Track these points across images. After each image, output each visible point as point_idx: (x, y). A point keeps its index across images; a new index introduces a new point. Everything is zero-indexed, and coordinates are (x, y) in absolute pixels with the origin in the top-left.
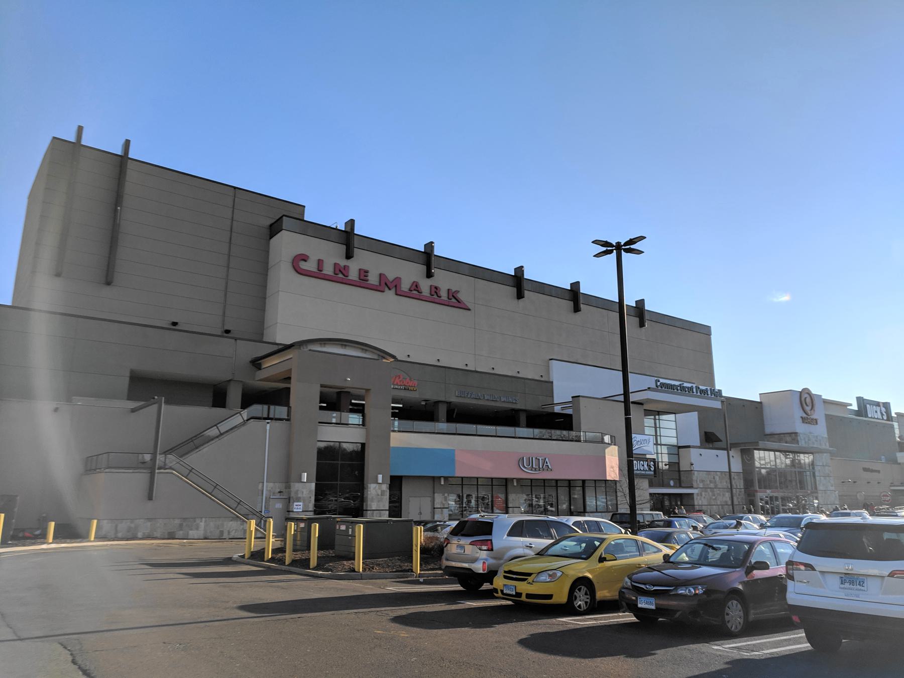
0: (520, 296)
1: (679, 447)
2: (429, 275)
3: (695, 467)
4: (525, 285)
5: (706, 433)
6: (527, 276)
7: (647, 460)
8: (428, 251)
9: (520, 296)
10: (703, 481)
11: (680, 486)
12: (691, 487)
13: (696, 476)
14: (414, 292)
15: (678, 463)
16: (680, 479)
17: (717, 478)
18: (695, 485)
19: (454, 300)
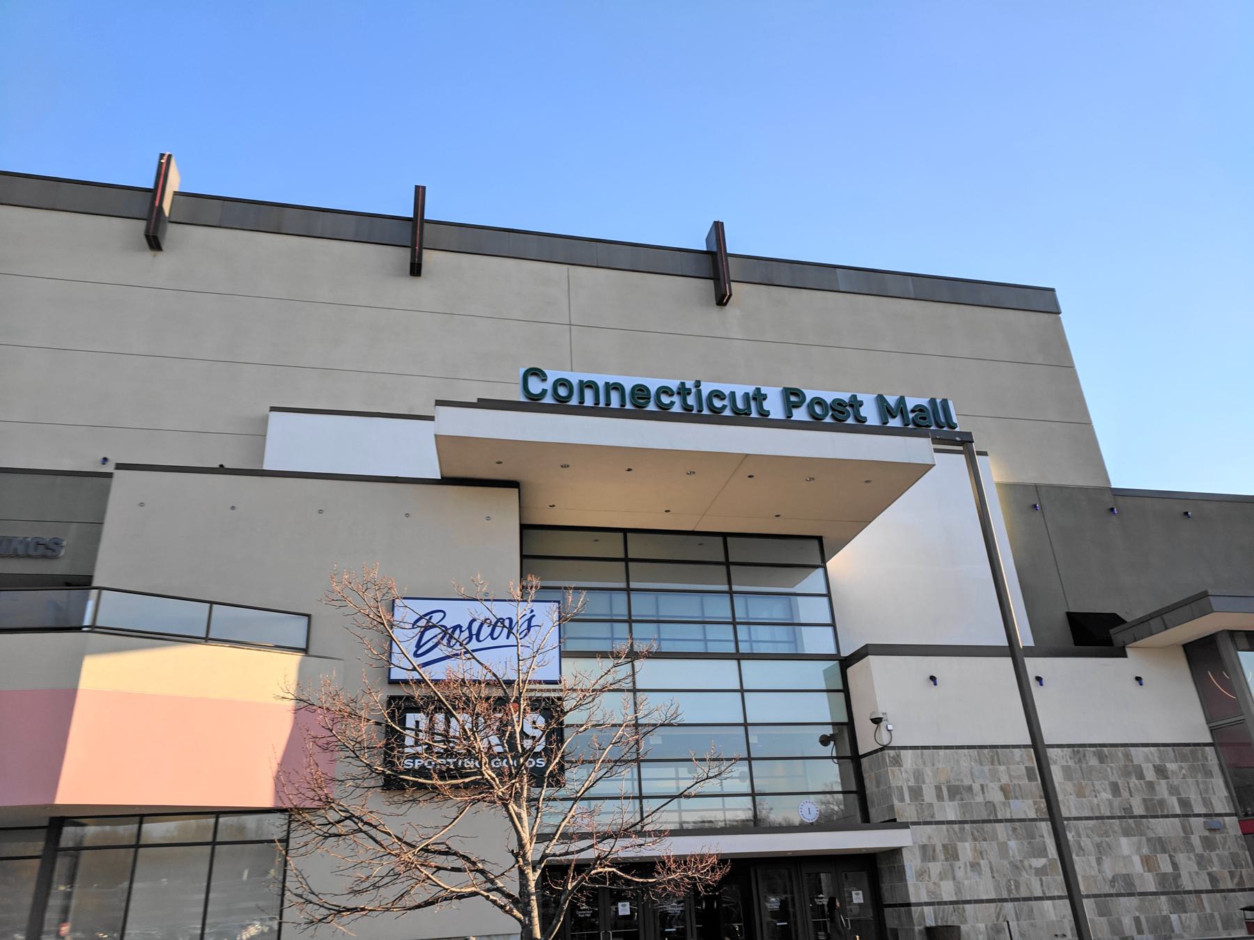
1: (845, 663)
4: (734, 268)
6: (734, 245)
13: (900, 777)
18: (906, 810)
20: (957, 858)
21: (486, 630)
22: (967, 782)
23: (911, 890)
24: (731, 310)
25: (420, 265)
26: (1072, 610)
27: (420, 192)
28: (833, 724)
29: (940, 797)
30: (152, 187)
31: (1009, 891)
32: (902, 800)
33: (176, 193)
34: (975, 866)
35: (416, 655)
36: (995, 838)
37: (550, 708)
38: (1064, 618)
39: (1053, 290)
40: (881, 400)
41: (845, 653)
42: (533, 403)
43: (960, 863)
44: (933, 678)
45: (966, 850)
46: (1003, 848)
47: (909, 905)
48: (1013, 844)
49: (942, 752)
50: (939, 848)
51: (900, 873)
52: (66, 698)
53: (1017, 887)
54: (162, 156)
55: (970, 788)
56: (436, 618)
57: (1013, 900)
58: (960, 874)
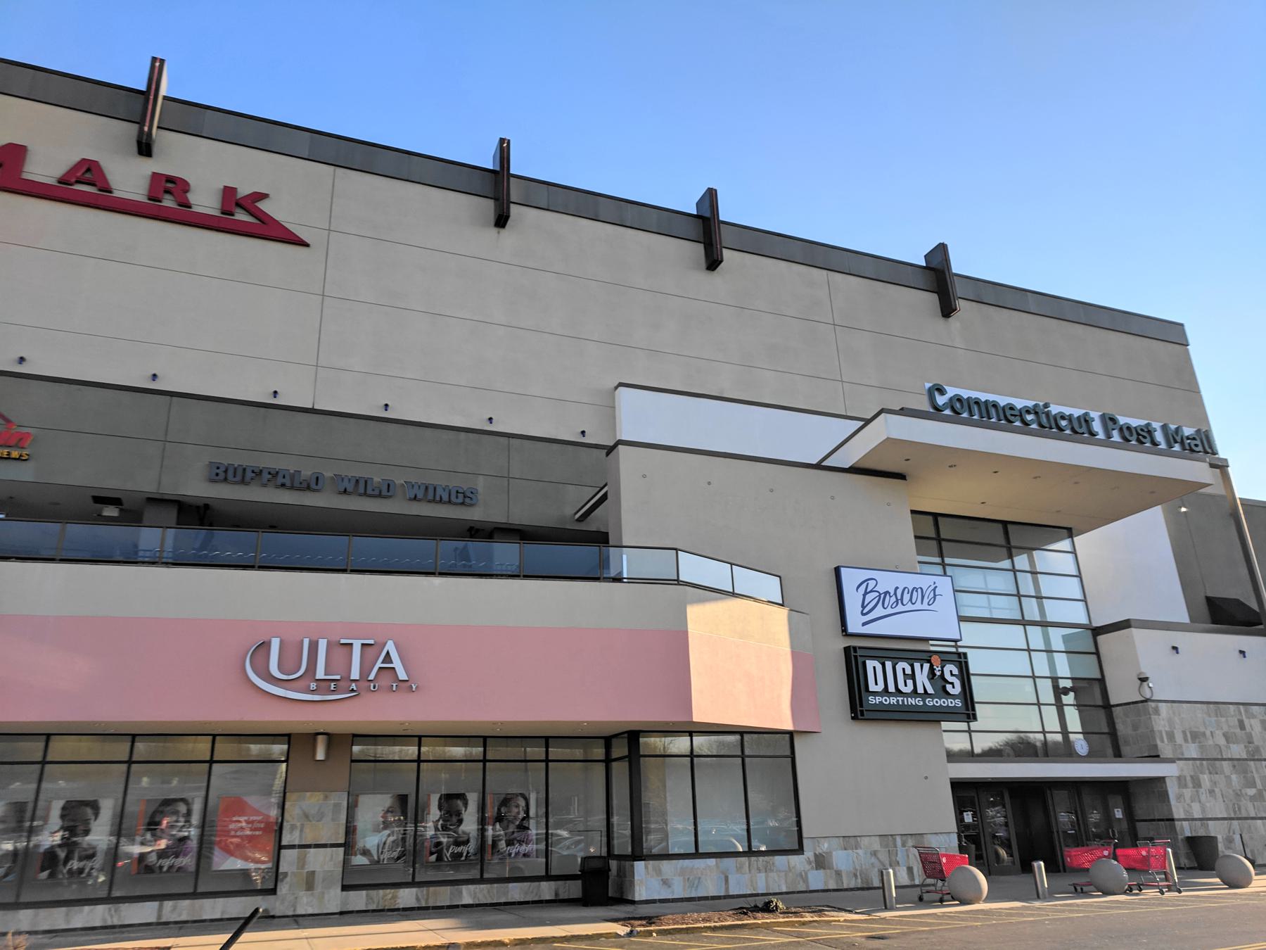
0: (947, 310)
1: (1097, 632)
2: (145, 148)
3: (1160, 689)
4: (726, 236)
5: (1209, 600)
6: (726, 213)
7: (926, 657)
8: (707, 214)
9: (947, 310)
10: (1196, 736)
11: (1118, 755)
12: (1155, 757)
13: (1161, 721)
14: (84, 187)
15: (1102, 681)
16: (1113, 734)
17: (1254, 726)
18: (1166, 749)
19: (244, 217)
20: (1200, 786)
21: (906, 597)
22: (1202, 729)
23: (1174, 809)
24: (954, 321)
25: (507, 217)
26: (1210, 594)
27: (157, 67)
28: (1072, 679)
29: (1186, 741)
30: (143, 88)
31: (1235, 812)
32: (1162, 741)
33: (165, 98)
34: (1212, 792)
35: (863, 614)
36: (1222, 772)
37: (962, 662)
38: (1204, 601)
39: (1182, 325)
40: (1165, 428)
41: (1096, 624)
42: (936, 413)
43: (1202, 790)
44: (1175, 648)
45: (1205, 779)
46: (1228, 778)
47: (1173, 820)
48: (1234, 777)
49: (1184, 705)
50: (1188, 778)
51: (1164, 796)
52: (678, 643)
53: (1239, 809)
54: (154, 59)
55: (1204, 734)
56: (872, 584)
57: (1238, 819)
58: (1203, 798)
